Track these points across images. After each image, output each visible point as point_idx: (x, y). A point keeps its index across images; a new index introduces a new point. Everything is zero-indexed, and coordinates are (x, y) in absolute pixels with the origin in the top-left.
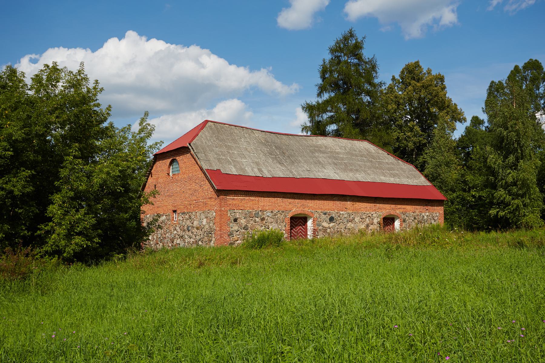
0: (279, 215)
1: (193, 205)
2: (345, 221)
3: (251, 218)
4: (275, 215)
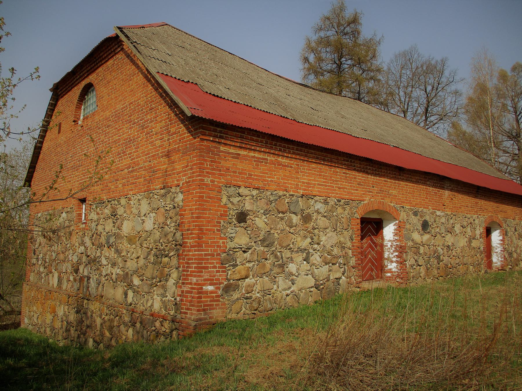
0: (340, 210)
3: (281, 215)
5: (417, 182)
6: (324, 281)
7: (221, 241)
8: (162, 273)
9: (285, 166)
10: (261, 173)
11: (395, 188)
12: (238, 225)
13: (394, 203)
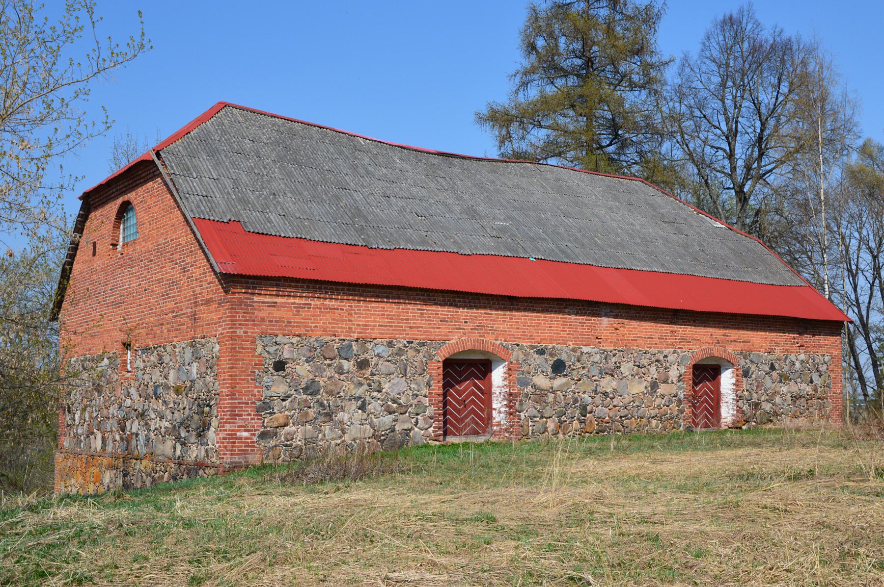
0: (411, 353)
1: (168, 324)
2: (595, 371)
3: (328, 362)
4: (400, 352)
5: (543, 311)
6: (387, 432)
7: (256, 390)
8: (204, 423)
9: (335, 309)
10: (302, 319)
11: (504, 321)
12: (275, 374)
13: (501, 340)
